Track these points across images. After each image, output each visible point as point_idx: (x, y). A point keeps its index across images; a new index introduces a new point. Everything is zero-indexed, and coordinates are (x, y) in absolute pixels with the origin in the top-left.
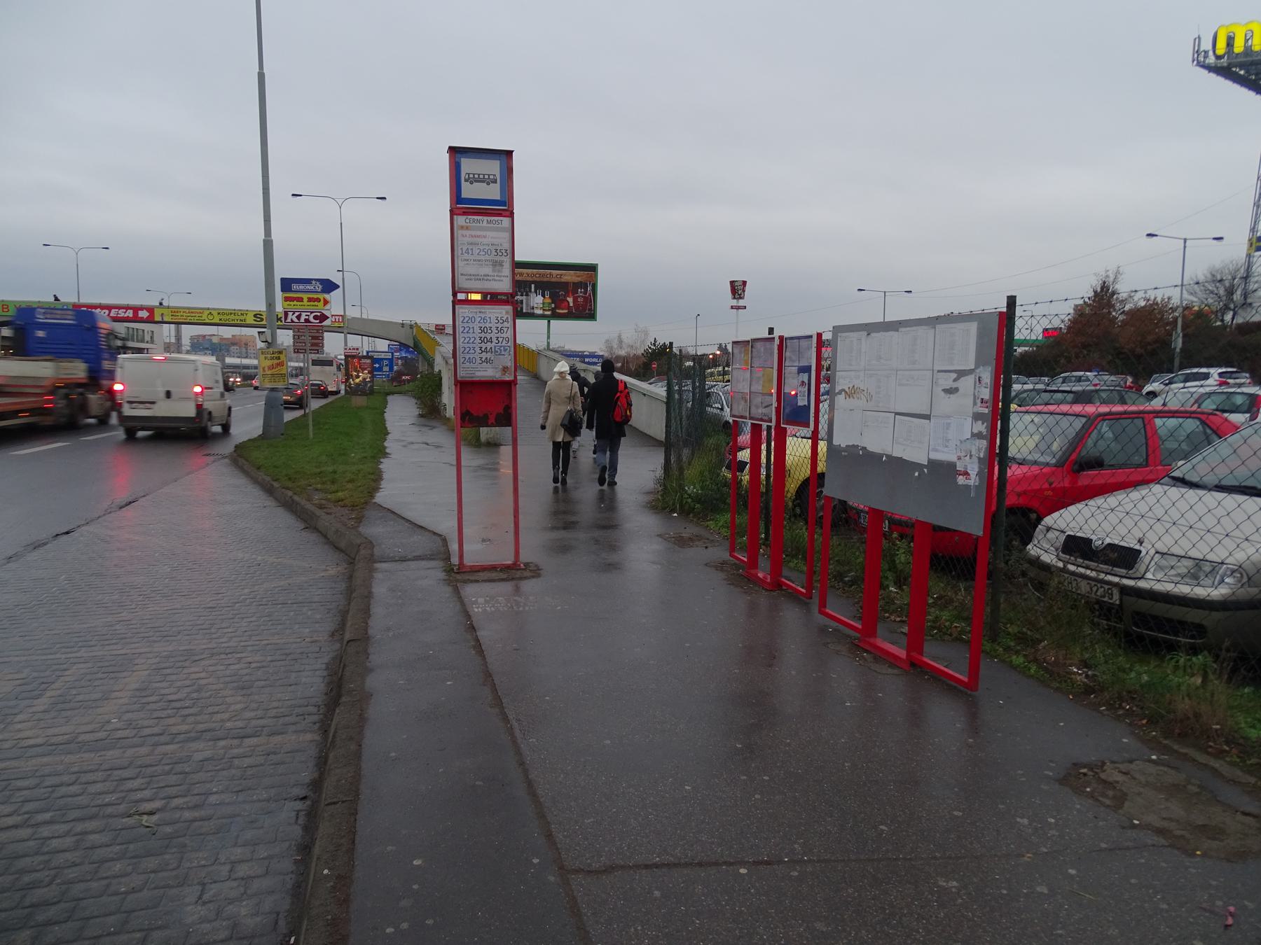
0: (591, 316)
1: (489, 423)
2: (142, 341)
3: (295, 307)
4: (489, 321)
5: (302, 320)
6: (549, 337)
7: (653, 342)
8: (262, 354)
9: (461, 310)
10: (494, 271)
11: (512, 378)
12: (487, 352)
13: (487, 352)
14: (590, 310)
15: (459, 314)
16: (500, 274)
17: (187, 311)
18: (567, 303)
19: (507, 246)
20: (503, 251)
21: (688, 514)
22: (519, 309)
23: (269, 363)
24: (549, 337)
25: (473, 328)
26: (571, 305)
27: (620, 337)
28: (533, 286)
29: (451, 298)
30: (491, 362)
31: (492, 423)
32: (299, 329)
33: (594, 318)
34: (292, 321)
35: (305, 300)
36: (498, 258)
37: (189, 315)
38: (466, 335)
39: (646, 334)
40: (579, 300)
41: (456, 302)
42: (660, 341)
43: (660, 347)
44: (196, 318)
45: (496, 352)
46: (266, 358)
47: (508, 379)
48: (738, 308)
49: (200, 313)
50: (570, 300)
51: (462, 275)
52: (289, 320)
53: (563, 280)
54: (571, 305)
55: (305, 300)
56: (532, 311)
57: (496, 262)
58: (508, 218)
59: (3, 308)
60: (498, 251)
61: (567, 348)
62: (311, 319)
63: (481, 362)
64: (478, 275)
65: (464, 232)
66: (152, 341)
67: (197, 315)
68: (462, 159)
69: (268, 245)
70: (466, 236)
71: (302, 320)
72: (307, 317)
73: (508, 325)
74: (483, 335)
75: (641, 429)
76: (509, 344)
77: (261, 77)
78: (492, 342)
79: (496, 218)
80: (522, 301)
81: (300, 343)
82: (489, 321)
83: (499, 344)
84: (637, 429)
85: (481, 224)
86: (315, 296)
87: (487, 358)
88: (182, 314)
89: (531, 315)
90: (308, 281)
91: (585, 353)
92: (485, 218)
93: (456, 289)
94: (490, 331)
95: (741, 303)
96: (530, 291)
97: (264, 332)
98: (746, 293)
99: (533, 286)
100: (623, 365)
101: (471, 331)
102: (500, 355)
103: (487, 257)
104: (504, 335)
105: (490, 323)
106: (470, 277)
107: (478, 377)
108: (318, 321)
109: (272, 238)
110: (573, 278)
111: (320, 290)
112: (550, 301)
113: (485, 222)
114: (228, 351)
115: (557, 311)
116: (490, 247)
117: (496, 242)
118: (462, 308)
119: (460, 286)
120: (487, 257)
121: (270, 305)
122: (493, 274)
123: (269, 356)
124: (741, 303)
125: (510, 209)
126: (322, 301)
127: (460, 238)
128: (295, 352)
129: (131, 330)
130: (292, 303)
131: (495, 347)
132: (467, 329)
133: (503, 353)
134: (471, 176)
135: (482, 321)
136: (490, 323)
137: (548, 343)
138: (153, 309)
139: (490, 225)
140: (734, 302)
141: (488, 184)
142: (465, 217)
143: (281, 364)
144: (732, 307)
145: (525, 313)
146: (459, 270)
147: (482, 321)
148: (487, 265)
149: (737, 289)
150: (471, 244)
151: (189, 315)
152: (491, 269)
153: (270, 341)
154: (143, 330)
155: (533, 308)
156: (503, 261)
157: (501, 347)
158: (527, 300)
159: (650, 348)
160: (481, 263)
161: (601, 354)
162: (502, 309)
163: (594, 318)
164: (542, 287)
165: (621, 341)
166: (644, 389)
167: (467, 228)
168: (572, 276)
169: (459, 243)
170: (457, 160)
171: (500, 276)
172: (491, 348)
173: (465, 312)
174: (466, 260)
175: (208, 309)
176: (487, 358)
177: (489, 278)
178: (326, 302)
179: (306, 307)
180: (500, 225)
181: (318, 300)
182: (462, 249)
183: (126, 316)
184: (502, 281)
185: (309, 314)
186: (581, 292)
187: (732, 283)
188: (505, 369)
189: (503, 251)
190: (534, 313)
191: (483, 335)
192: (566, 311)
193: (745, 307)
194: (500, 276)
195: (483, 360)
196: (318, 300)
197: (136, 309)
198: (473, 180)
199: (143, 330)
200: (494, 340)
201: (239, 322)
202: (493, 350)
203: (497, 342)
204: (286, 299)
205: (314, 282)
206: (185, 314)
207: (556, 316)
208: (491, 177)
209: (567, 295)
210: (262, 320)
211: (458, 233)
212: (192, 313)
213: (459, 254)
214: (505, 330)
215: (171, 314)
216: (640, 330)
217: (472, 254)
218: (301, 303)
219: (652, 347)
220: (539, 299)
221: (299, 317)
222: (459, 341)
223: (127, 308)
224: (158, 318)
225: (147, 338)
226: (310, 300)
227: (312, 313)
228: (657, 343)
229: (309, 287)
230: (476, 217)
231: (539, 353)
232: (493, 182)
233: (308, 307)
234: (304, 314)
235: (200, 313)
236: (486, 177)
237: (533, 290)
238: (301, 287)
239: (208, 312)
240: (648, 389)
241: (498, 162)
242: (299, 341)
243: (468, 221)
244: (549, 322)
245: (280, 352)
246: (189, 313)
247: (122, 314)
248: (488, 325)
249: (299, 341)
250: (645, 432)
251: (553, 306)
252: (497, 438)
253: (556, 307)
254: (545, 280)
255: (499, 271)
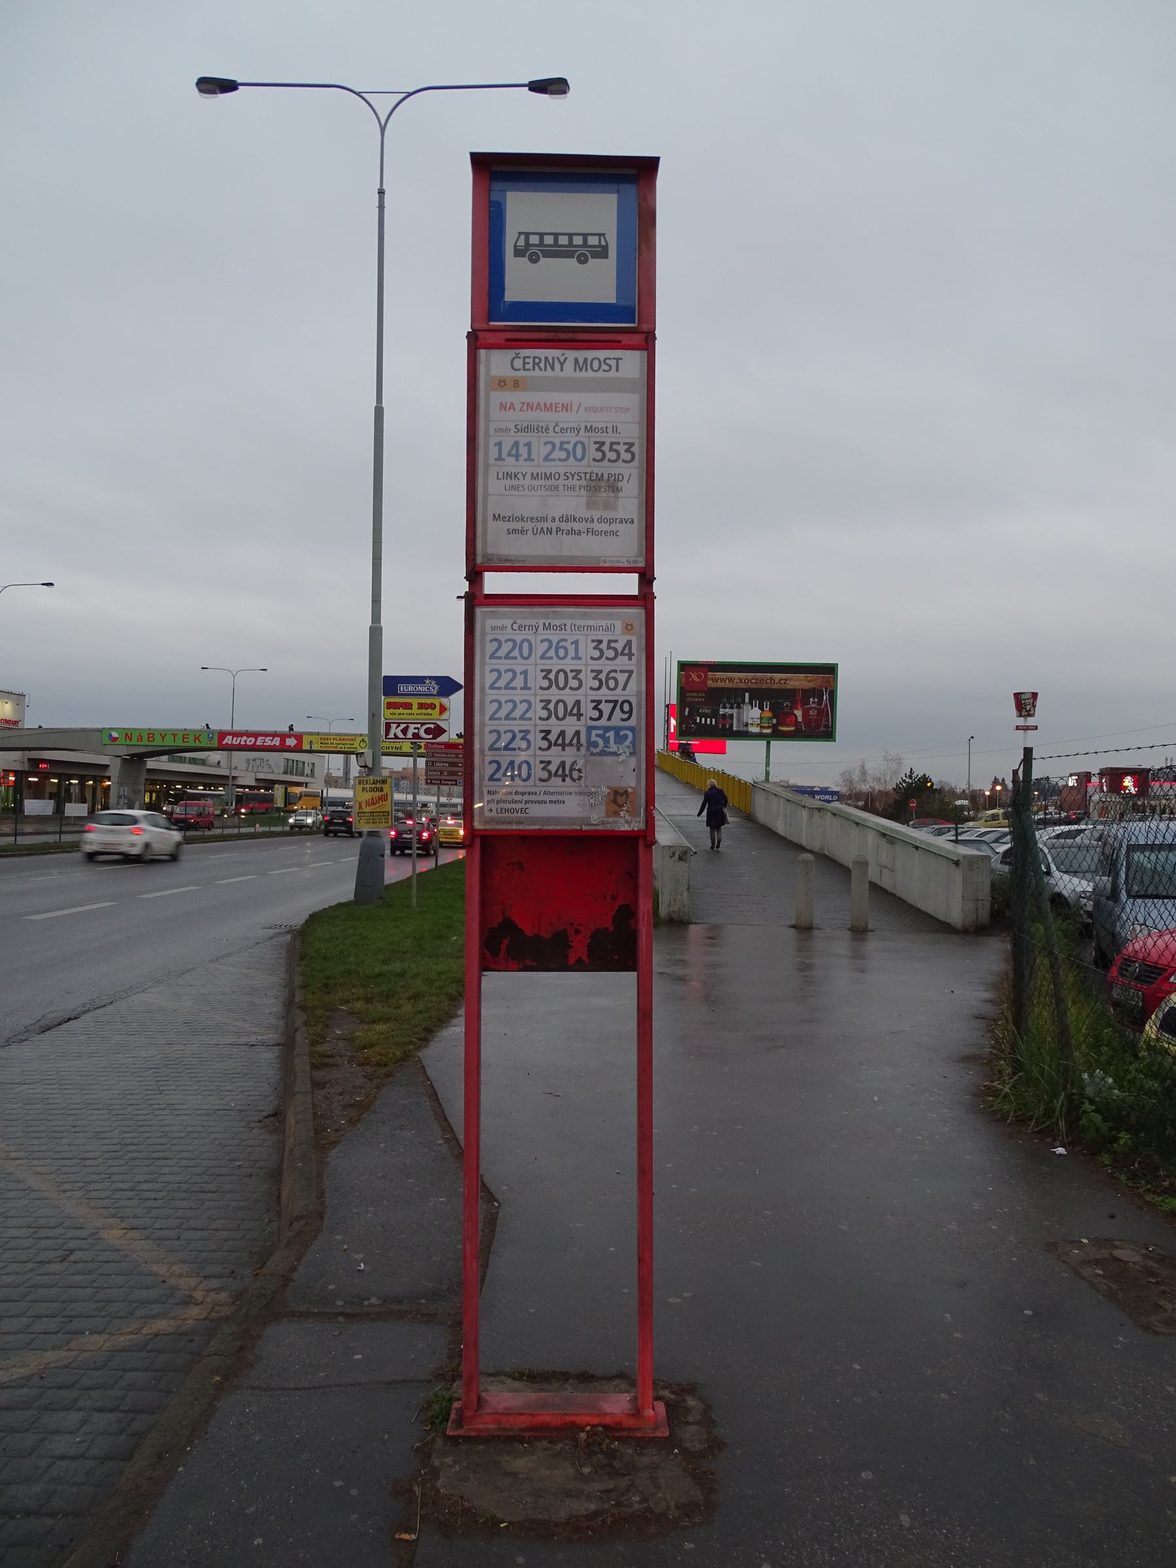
0: (828, 734)
1: (572, 960)
2: (302, 775)
3: (401, 716)
4: (572, 653)
5: (410, 735)
6: (768, 764)
7: (908, 774)
8: (360, 783)
9: (490, 622)
10: (590, 505)
11: (638, 825)
12: (563, 746)
13: (563, 746)
14: (827, 726)
15: (484, 634)
16: (610, 514)
17: (338, 738)
18: (793, 718)
19: (632, 431)
20: (622, 448)
21: (989, 1031)
22: (727, 726)
23: (368, 796)
24: (768, 764)
25: (525, 673)
26: (800, 719)
27: (863, 767)
28: (747, 695)
29: (465, 587)
30: (575, 774)
31: (580, 961)
32: (433, 753)
33: (832, 738)
34: (396, 737)
35: (415, 706)
36: (604, 469)
37: (340, 742)
38: (503, 696)
39: (899, 761)
40: (811, 713)
41: (474, 600)
42: (919, 773)
43: (919, 780)
44: (346, 746)
45: (591, 744)
46: (364, 789)
47: (625, 827)
48: (1026, 728)
49: (352, 740)
50: (798, 713)
51: (496, 518)
52: (391, 735)
53: (788, 687)
54: (800, 719)
55: (415, 706)
56: (745, 729)
57: (600, 478)
58: (637, 353)
59: (149, 737)
60: (606, 448)
61: (792, 782)
62: (422, 734)
63: (545, 775)
64: (545, 519)
65: (508, 396)
66: (312, 775)
67: (348, 742)
68: (509, 194)
69: (376, 634)
70: (512, 406)
71: (410, 735)
72: (416, 731)
73: (631, 665)
74: (554, 694)
75: (911, 902)
76: (632, 722)
77: (379, 412)
78: (579, 715)
79: (602, 354)
80: (731, 716)
81: (435, 771)
82: (572, 653)
83: (603, 722)
84: (904, 901)
85: (557, 372)
86: (429, 701)
87: (563, 764)
88: (332, 741)
89: (744, 735)
90: (419, 680)
91: (815, 789)
92: (571, 355)
93: (479, 560)
94: (575, 683)
95: (1031, 721)
96: (744, 702)
97: (363, 753)
98: (1037, 708)
99: (747, 695)
100: (866, 803)
101: (519, 682)
102: (603, 753)
103: (572, 466)
104: (619, 695)
105: (577, 657)
106: (518, 525)
107: (534, 820)
108: (431, 736)
109: (382, 624)
110: (804, 683)
111: (435, 692)
112: (770, 715)
113: (570, 364)
114: (397, 785)
115: (780, 728)
116: (583, 436)
117: (597, 420)
118: (495, 615)
119: (490, 550)
120: (572, 466)
121: (373, 716)
122: (587, 515)
123: (368, 786)
124: (1031, 721)
125: (645, 327)
126: (438, 706)
127: (496, 413)
128: (427, 783)
129: (290, 763)
130: (397, 711)
131: (590, 729)
132: (507, 677)
133: (613, 748)
134: (534, 240)
135: (552, 653)
136: (577, 657)
137: (767, 773)
138: (302, 736)
139: (583, 374)
140: (1021, 721)
141: (582, 260)
142: (511, 353)
143: (384, 798)
144: (1018, 728)
145: (736, 731)
146: (490, 505)
147: (552, 653)
148: (572, 488)
149: (1025, 704)
150: (528, 429)
151: (340, 742)
152: (584, 500)
153: (370, 765)
154: (304, 762)
155: (747, 725)
156: (618, 478)
157: (607, 729)
158: (739, 713)
159: (904, 781)
160: (553, 482)
161: (836, 789)
162: (610, 616)
163: (832, 738)
164: (759, 696)
165: (864, 773)
166: (915, 839)
167: (517, 384)
168: (801, 680)
169: (493, 426)
170: (495, 196)
171: (611, 521)
172: (577, 733)
173: (503, 628)
174: (508, 475)
175: (361, 735)
176: (563, 764)
177: (576, 526)
178: (443, 709)
179: (415, 717)
180: (612, 373)
181: (433, 706)
182: (499, 444)
183: (272, 744)
184: (615, 533)
185: (419, 726)
186: (814, 702)
187: (1017, 696)
188: (618, 798)
189: (622, 448)
190: (748, 732)
191: (554, 694)
192: (793, 729)
193: (1036, 728)
194: (611, 521)
195: (553, 768)
196: (433, 706)
197: (283, 737)
198: (532, 252)
199: (304, 762)
200: (588, 711)
201: (394, 750)
202: (583, 740)
203: (596, 714)
204: (390, 706)
205: (428, 681)
206: (335, 742)
207: (778, 735)
208: (593, 241)
209: (794, 706)
210: (420, 747)
211: (490, 400)
212: (343, 740)
213: (492, 461)
214: (622, 678)
215: (320, 741)
216: (890, 757)
217: (529, 459)
218: (409, 711)
219: (907, 780)
220: (755, 713)
221: (405, 731)
222: (482, 713)
223: (274, 735)
224: (306, 746)
225: (307, 771)
226: (421, 706)
227: (423, 724)
228: (914, 775)
229: (421, 688)
230: (541, 353)
231: (754, 786)
232: (596, 255)
233: (418, 717)
234: (412, 727)
235: (352, 740)
236: (578, 240)
237: (747, 700)
238: (411, 688)
239: (360, 739)
240: (922, 838)
241: (614, 196)
242: (433, 768)
243: (518, 363)
244: (768, 743)
245: (384, 782)
246: (340, 739)
247: (268, 742)
248: (569, 665)
249: (433, 768)
250: (919, 906)
251: (774, 721)
252: (684, 912)
253: (779, 723)
254: (764, 686)
255: (607, 506)
